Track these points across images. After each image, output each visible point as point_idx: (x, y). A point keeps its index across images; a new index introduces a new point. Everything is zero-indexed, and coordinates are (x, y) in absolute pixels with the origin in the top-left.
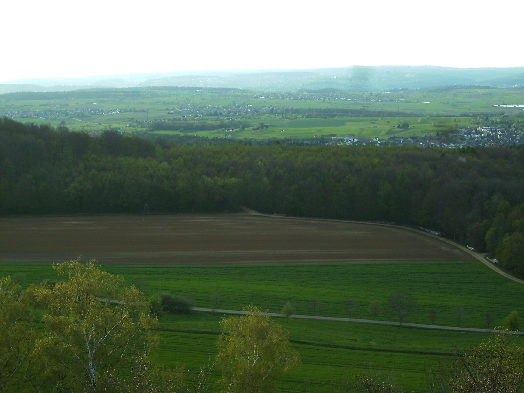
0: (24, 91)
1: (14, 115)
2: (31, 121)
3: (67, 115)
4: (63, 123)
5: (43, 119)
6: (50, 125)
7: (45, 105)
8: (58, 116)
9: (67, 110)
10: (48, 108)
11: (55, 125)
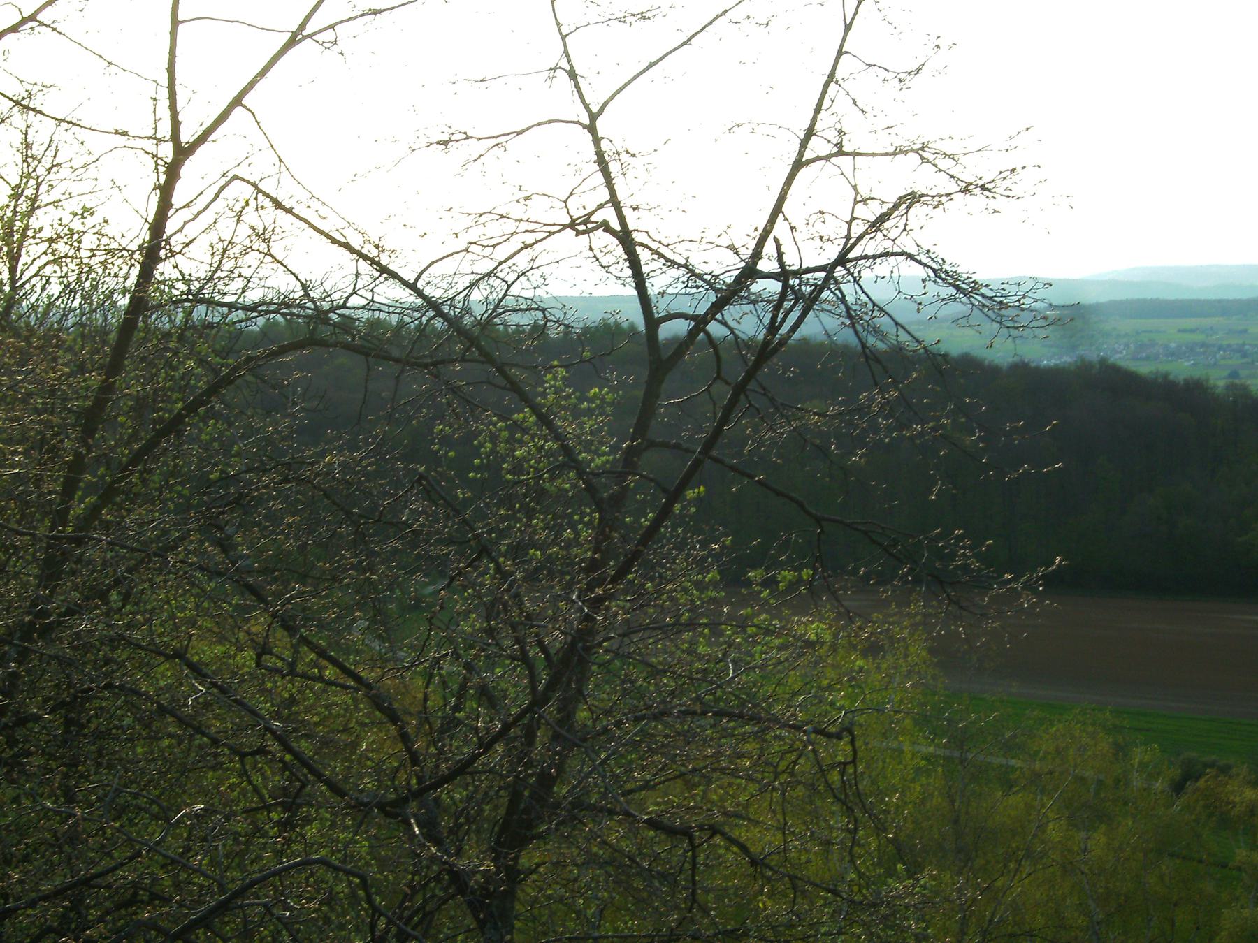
0: (1238, 297)
1: (1117, 352)
2: (1163, 368)
3: (1244, 355)
4: (1234, 374)
5: (1186, 364)
6: (1208, 380)
7: (1192, 331)
8: (1223, 358)
9: (1244, 345)
10: (1199, 337)
11: (1218, 381)
